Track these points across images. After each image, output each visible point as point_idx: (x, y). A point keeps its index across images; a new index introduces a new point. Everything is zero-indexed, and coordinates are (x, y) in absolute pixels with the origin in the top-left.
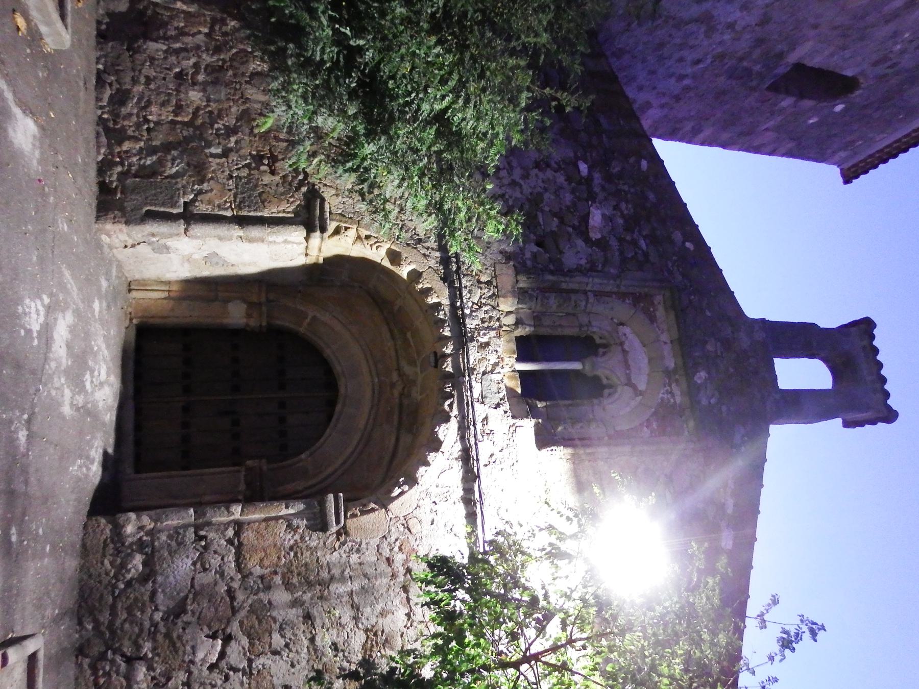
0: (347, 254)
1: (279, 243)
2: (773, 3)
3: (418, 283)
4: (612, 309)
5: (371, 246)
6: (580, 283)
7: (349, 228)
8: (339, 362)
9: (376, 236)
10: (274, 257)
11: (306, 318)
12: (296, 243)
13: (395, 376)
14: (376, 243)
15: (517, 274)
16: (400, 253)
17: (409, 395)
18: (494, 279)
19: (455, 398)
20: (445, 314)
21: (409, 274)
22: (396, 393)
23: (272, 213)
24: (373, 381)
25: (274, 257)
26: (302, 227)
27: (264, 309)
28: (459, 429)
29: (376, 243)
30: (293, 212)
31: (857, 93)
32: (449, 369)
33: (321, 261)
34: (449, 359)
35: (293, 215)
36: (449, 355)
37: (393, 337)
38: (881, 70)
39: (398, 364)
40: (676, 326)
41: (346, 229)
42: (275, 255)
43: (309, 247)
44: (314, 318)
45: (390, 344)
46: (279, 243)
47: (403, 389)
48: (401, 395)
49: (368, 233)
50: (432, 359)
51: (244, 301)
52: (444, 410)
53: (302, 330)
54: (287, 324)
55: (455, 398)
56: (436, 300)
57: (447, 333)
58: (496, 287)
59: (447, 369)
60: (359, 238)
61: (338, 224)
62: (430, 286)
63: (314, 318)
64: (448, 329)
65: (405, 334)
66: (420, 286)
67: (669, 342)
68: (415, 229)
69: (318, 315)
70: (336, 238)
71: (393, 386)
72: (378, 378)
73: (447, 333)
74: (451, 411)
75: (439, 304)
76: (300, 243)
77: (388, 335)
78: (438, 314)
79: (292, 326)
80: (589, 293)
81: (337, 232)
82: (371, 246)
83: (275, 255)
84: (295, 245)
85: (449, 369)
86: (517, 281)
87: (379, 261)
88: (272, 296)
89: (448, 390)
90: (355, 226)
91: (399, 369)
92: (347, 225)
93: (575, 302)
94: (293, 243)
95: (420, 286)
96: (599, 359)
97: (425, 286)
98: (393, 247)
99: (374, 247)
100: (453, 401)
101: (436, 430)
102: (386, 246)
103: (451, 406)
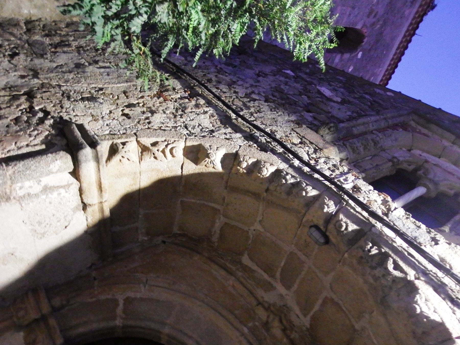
0: (136, 187)
1: (37, 195)
2: (229, 176)
3: (239, 163)
4: (396, 140)
5: (163, 152)
6: (364, 124)
7: (127, 142)
8: (186, 334)
9: (163, 139)
10: (37, 227)
11: (118, 305)
12: (62, 187)
13: (262, 314)
14: (166, 146)
15: (317, 132)
16: (200, 145)
17: (292, 326)
18: (303, 139)
19: (393, 255)
20: (293, 176)
21: (223, 161)
22: (277, 331)
23: (9, 151)
24: (243, 334)
25: (37, 227)
26: (62, 153)
27: (52, 322)
28: (436, 290)
29: (166, 146)
30: (42, 143)
31: (365, 40)
32: (352, 227)
33: (107, 213)
34: (341, 216)
35: (43, 147)
36: (337, 212)
37: (230, 273)
38: (372, 20)
39: (256, 299)
40: (445, 131)
41: (124, 144)
42: (40, 223)
43: (85, 186)
44: (128, 301)
45: (231, 281)
46: (37, 195)
47: (281, 321)
48: (284, 330)
49: (154, 140)
50: (316, 234)
51: (19, 328)
52: (395, 280)
53: (118, 322)
54: (95, 326)
55: (393, 255)
56: (272, 169)
57: (312, 192)
58: (311, 143)
59: (350, 229)
60: (144, 149)
61: (110, 142)
62: (255, 160)
63: (128, 301)
64: (309, 188)
65: (240, 263)
66: (244, 165)
67: (452, 145)
68: (200, 125)
69: (132, 295)
70: (116, 158)
71: (266, 325)
72: (245, 326)
73: (312, 192)
74: (406, 274)
75: (278, 172)
76: (68, 186)
77: (223, 273)
78: (286, 180)
79: (103, 325)
80: (374, 132)
81: (113, 151)
82: (163, 152)
83: (40, 223)
84: (62, 191)
85: (352, 227)
86: (322, 136)
87: (179, 173)
88: (57, 302)
89: (374, 251)
90: (134, 138)
91: (259, 303)
92: (123, 140)
93: (373, 140)
94: (58, 187)
95: (244, 165)
96: (431, 176)
97: (250, 162)
98: (189, 144)
99: (167, 151)
100: (392, 258)
101: (418, 311)
102: (180, 147)
103: (397, 267)
